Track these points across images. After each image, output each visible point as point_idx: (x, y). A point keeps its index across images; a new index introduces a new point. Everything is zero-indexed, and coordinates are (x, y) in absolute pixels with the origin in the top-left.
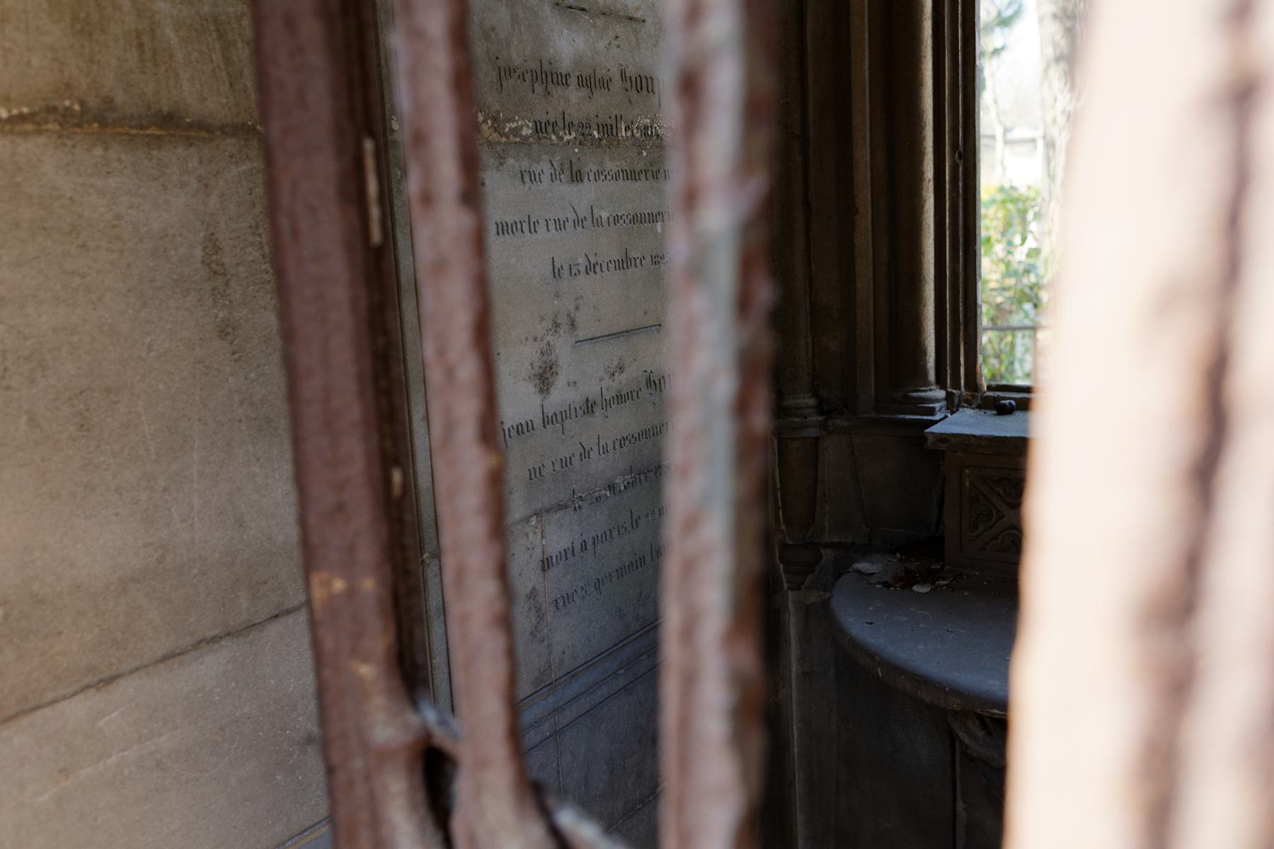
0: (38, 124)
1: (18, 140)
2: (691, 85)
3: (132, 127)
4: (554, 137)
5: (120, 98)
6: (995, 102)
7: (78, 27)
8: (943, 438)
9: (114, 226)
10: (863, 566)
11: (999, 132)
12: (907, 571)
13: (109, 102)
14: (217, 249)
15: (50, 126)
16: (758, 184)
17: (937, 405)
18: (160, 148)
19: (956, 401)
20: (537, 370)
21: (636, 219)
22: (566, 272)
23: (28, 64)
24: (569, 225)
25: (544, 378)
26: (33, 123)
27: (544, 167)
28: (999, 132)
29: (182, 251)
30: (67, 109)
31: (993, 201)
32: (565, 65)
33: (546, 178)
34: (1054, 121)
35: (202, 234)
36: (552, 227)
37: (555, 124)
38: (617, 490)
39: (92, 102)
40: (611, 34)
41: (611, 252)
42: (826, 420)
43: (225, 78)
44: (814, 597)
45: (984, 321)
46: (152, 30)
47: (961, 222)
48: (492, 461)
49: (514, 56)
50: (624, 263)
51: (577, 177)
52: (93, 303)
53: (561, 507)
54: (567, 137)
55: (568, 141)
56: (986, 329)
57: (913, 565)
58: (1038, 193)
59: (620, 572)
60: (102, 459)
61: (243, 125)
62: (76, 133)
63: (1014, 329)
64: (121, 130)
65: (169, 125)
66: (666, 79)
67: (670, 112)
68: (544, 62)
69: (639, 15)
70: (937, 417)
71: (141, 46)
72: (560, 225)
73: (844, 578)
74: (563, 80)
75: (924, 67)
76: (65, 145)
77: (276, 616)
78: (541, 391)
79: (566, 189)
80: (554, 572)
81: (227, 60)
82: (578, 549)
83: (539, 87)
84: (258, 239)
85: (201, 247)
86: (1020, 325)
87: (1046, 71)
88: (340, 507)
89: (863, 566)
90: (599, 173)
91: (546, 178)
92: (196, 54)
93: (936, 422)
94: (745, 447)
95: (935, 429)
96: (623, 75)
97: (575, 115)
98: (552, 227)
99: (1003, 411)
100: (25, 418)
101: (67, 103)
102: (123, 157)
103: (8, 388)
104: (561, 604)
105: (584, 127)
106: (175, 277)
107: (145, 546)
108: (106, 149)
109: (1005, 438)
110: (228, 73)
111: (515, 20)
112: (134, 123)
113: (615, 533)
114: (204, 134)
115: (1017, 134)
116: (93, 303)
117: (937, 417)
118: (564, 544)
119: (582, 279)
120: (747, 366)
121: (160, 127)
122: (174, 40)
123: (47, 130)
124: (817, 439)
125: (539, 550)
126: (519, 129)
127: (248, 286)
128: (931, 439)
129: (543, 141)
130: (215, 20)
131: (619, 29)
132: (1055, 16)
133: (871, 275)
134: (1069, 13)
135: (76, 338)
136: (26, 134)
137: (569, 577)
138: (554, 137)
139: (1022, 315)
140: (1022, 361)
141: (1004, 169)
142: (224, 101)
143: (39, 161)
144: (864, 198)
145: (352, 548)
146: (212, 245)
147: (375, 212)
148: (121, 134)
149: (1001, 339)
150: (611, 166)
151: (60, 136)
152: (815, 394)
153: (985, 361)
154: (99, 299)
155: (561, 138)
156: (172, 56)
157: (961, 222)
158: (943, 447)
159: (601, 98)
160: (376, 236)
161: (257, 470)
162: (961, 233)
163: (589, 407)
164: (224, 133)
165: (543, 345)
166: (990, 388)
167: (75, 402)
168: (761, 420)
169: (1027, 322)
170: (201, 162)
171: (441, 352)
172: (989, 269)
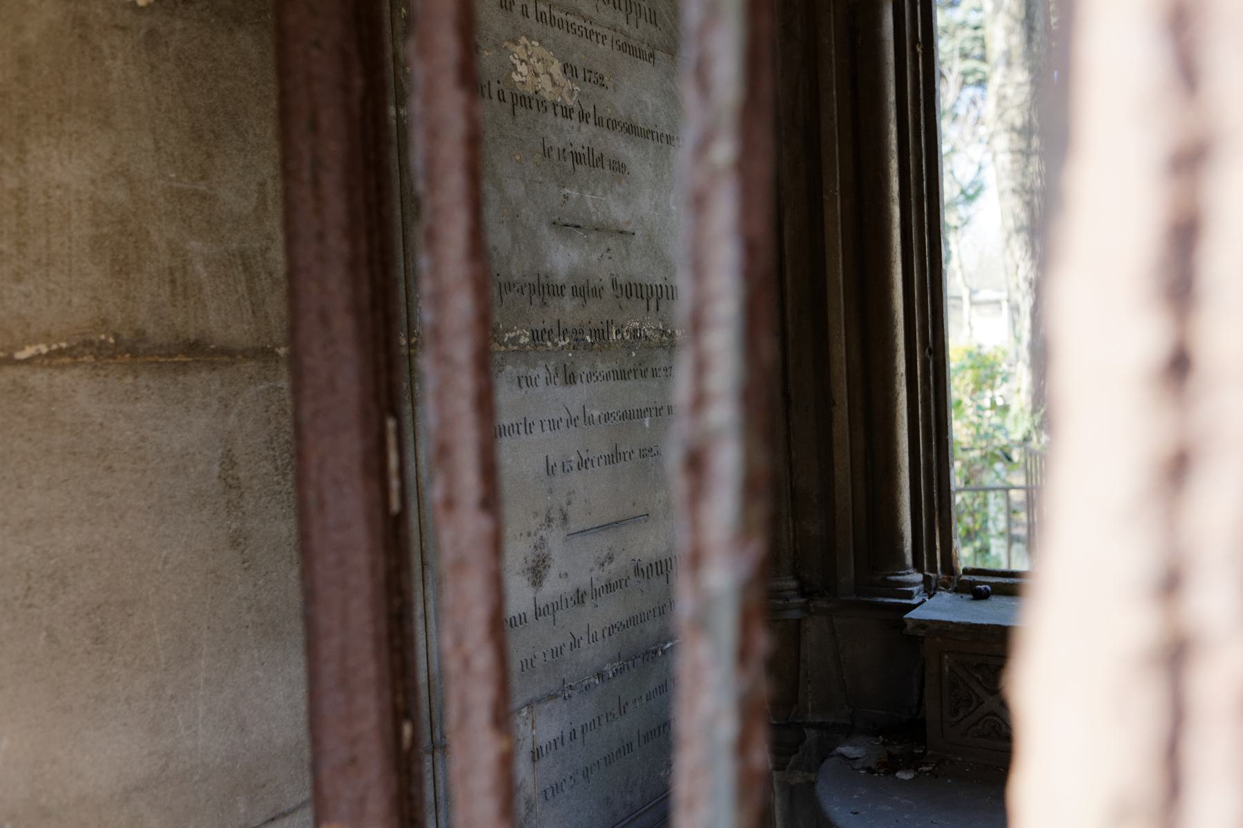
0: (75, 357)
1: (56, 373)
2: (696, 463)
3: (160, 356)
4: (549, 344)
5: (151, 329)
6: (961, 267)
7: (117, 268)
8: (922, 624)
9: (140, 448)
10: (845, 750)
11: (965, 294)
12: (890, 756)
13: (140, 334)
14: (233, 464)
15: (85, 359)
16: (757, 548)
17: (915, 589)
18: (185, 373)
19: (933, 584)
20: (530, 564)
21: (626, 416)
22: (559, 468)
23: (70, 303)
24: (563, 425)
25: (537, 572)
26: (70, 356)
27: (541, 372)
28: (965, 294)
29: (201, 468)
30: (102, 342)
31: (963, 367)
32: (561, 276)
33: (541, 382)
34: (1018, 286)
35: (220, 451)
36: (546, 427)
37: (550, 332)
38: (605, 678)
39: (126, 335)
40: (603, 247)
41: (602, 448)
42: (808, 602)
43: (249, 307)
44: (798, 778)
45: (956, 480)
46: (184, 267)
47: (933, 413)
48: (504, 744)
49: (514, 272)
50: (614, 457)
51: (570, 379)
52: (115, 521)
53: (552, 697)
54: (562, 343)
55: (563, 347)
56: (960, 490)
57: (896, 749)
58: (1005, 353)
59: (608, 760)
60: (114, 670)
61: (263, 348)
62: (108, 364)
63: (987, 490)
64: (151, 359)
65: (196, 352)
66: (673, 458)
67: (678, 484)
68: (542, 276)
69: (629, 228)
70: (915, 601)
71: (173, 282)
72: (554, 425)
73: (830, 763)
74: (558, 291)
75: (894, 271)
76: (98, 375)
77: (273, 819)
78: (534, 584)
79: (560, 391)
80: (543, 762)
81: (251, 291)
82: (567, 738)
83: (536, 300)
84: (271, 453)
85: (218, 463)
86: (992, 485)
87: (1008, 240)
88: (353, 761)
89: (845, 750)
90: (591, 374)
91: (541, 382)
92: (222, 287)
93: (915, 606)
94: (746, 782)
95: (914, 614)
96: (614, 283)
97: (569, 323)
98: (546, 427)
99: (980, 596)
100: (44, 634)
101: (103, 337)
102: (151, 384)
103: (30, 606)
104: (550, 794)
105: (577, 334)
106: (193, 492)
107: (150, 754)
108: (136, 377)
109: (982, 625)
110: (252, 303)
111: (515, 239)
112: (163, 352)
113: (603, 720)
114: (226, 359)
115: (982, 296)
116: (115, 521)
117: (915, 601)
118: (555, 734)
119: (575, 474)
120: (747, 710)
121: (187, 354)
122: (204, 275)
123: (83, 362)
124: (799, 620)
125: (529, 741)
126: (517, 338)
127: (261, 497)
128: (910, 624)
129: (539, 348)
130: (242, 255)
131: (611, 242)
132: (1014, 191)
133: (849, 463)
134: (1027, 187)
135: (97, 555)
136: (62, 367)
137: (558, 767)
138: (549, 344)
139: (993, 475)
140: (995, 520)
141: (971, 328)
142: (246, 327)
143: (74, 391)
144: (841, 391)
145: (362, 801)
146: (229, 461)
147: (395, 484)
148: (150, 363)
149: (974, 499)
150: (602, 367)
151: (94, 367)
152: (797, 577)
153: (959, 520)
154: (121, 517)
155: (556, 345)
156: (200, 289)
157: (933, 413)
158: (921, 633)
159: (593, 306)
160: (395, 505)
161: (261, 674)
162: (933, 423)
163: (579, 597)
164: (245, 357)
165: (536, 539)
166: (966, 571)
167: (92, 616)
168: (761, 757)
169: (998, 483)
170: (222, 385)
171: (459, 642)
172: (960, 431)
